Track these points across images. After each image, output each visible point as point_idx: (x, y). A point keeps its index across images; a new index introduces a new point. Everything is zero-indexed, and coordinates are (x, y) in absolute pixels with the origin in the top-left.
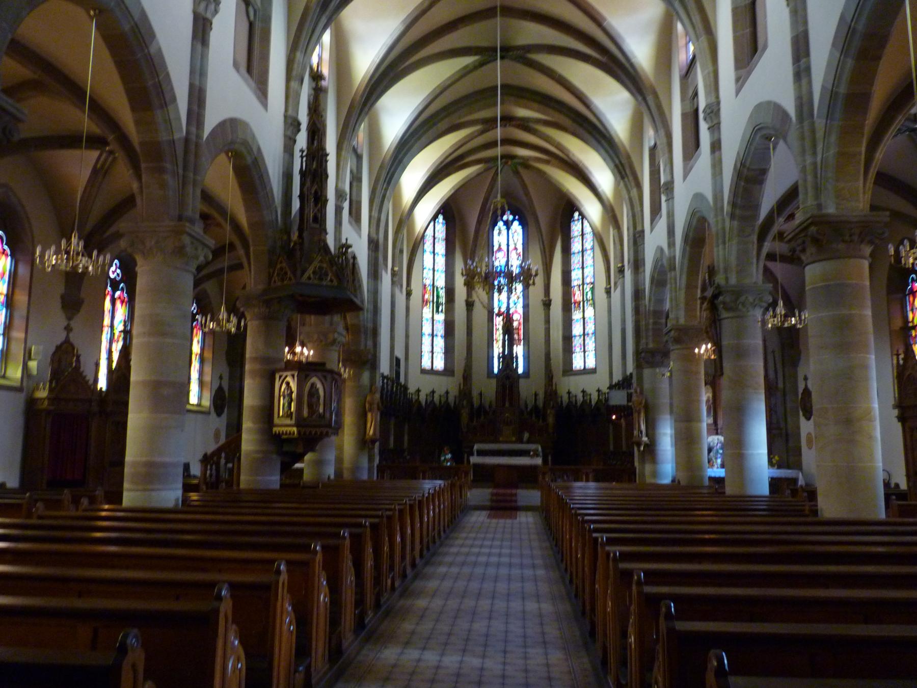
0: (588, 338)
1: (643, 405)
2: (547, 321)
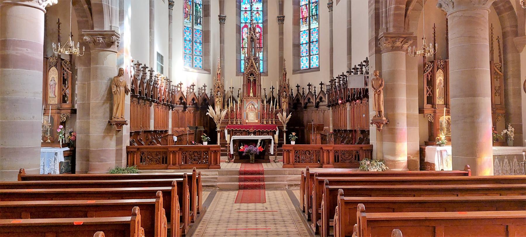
0: (313, 45)
1: (382, 87)
2: (281, 33)
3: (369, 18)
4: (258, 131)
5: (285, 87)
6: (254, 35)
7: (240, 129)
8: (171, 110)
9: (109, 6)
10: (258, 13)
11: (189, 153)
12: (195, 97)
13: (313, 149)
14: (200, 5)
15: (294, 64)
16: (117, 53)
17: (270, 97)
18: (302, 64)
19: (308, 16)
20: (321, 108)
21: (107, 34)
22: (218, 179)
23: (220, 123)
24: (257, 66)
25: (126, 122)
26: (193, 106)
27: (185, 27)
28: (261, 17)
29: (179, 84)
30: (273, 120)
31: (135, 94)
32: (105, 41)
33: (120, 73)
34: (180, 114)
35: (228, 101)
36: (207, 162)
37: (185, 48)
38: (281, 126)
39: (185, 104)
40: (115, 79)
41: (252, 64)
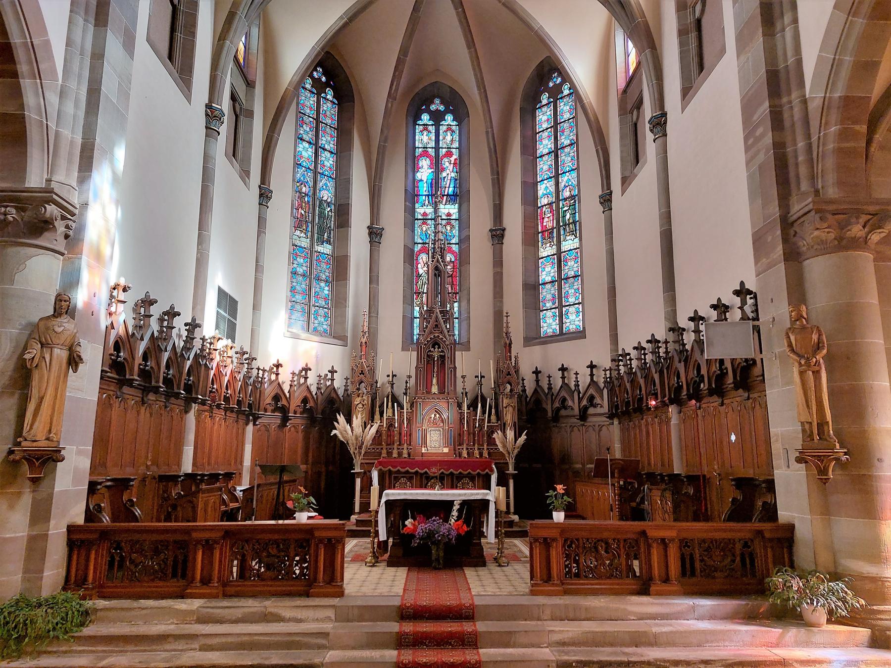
2: (498, 262)
3: (750, 178)
4: (448, 475)
5: (509, 372)
7: (406, 469)
8: (251, 424)
9: (47, 124)
10: (449, 223)
11: (254, 545)
12: (308, 395)
13: (619, 537)
14: (329, 204)
15: (527, 325)
16: (62, 254)
17: (474, 396)
18: (545, 325)
19: (555, 226)
20: (592, 420)
21: (31, 197)
22: (331, 637)
23: (362, 454)
24: (448, 327)
25: (60, 451)
26: (305, 416)
27: (296, 246)
28: (456, 232)
29: (273, 365)
30: (483, 449)
31: (127, 377)
32: (24, 219)
33: (57, 307)
34: (273, 433)
35: (381, 406)
36: (305, 575)
37: (293, 290)
38: (503, 463)
39: (284, 410)
40: (41, 325)
41: (437, 321)
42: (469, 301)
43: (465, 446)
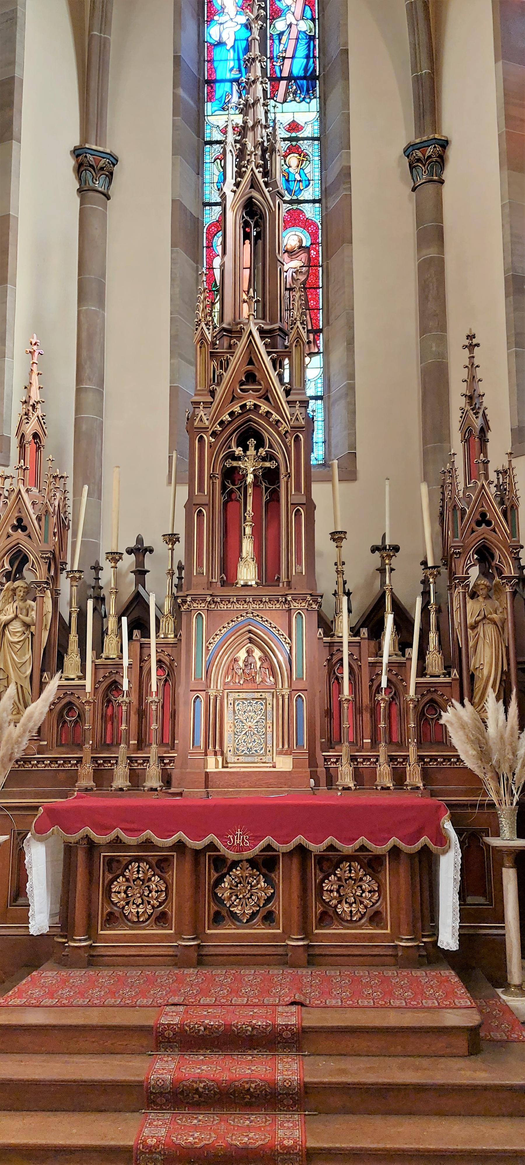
6: (267, 184)
28: (313, 170)
30: (406, 758)
41: (251, 362)
42: (350, 342)
43: (345, 750)
